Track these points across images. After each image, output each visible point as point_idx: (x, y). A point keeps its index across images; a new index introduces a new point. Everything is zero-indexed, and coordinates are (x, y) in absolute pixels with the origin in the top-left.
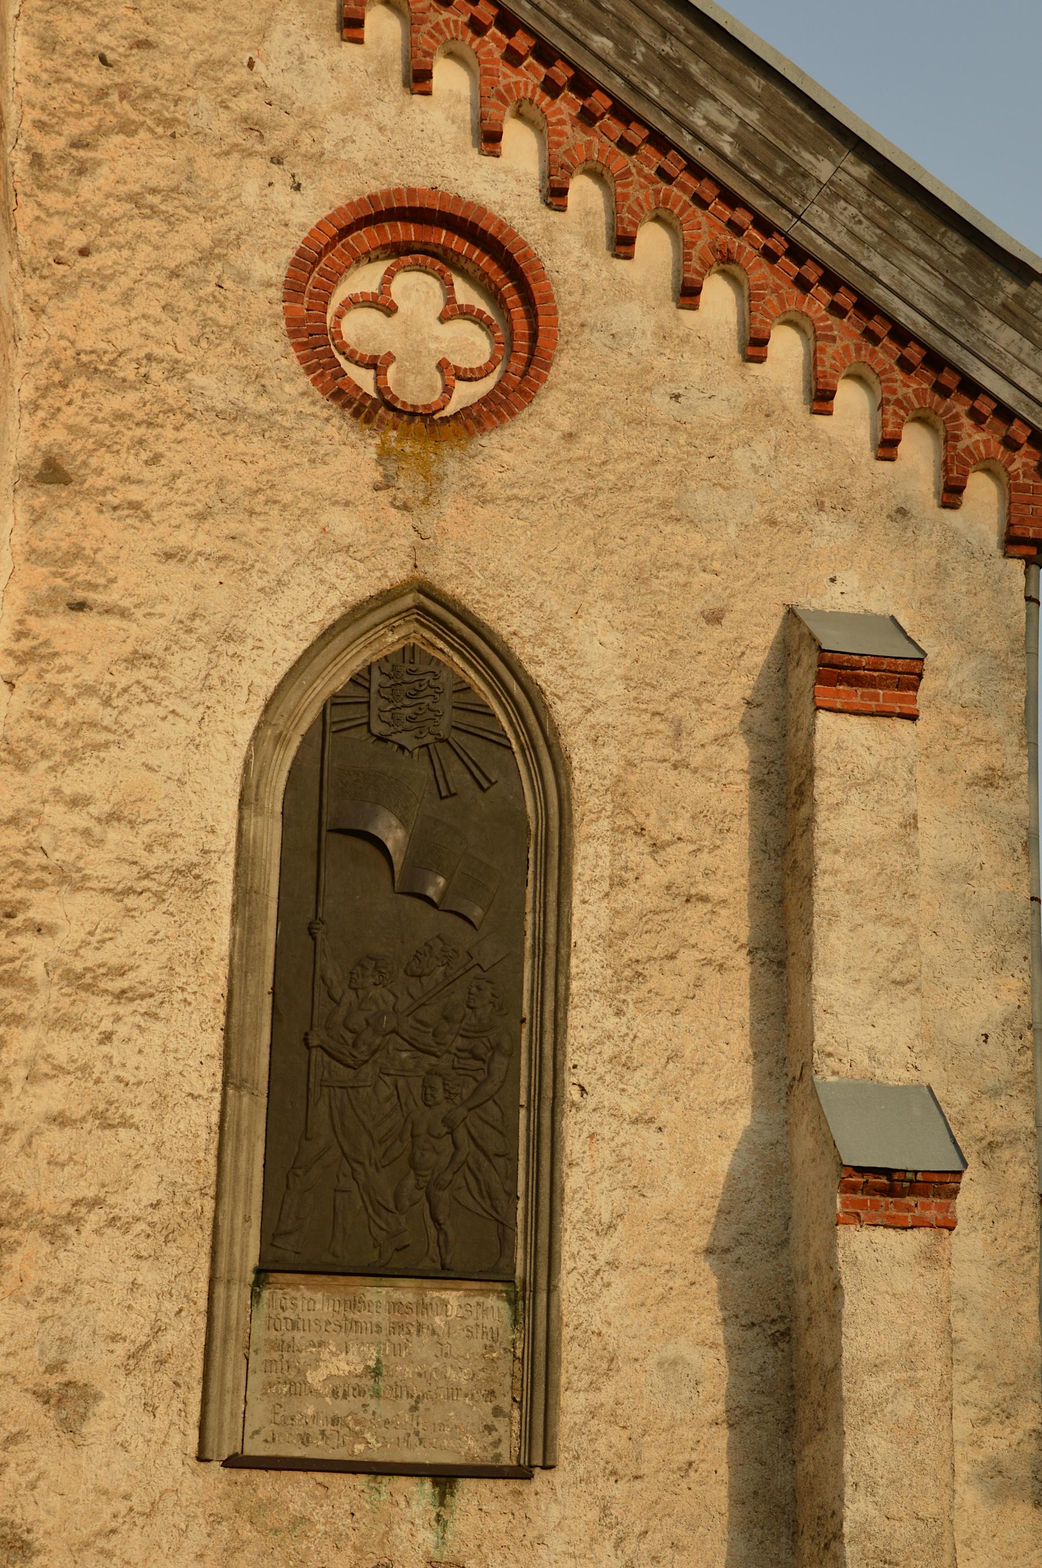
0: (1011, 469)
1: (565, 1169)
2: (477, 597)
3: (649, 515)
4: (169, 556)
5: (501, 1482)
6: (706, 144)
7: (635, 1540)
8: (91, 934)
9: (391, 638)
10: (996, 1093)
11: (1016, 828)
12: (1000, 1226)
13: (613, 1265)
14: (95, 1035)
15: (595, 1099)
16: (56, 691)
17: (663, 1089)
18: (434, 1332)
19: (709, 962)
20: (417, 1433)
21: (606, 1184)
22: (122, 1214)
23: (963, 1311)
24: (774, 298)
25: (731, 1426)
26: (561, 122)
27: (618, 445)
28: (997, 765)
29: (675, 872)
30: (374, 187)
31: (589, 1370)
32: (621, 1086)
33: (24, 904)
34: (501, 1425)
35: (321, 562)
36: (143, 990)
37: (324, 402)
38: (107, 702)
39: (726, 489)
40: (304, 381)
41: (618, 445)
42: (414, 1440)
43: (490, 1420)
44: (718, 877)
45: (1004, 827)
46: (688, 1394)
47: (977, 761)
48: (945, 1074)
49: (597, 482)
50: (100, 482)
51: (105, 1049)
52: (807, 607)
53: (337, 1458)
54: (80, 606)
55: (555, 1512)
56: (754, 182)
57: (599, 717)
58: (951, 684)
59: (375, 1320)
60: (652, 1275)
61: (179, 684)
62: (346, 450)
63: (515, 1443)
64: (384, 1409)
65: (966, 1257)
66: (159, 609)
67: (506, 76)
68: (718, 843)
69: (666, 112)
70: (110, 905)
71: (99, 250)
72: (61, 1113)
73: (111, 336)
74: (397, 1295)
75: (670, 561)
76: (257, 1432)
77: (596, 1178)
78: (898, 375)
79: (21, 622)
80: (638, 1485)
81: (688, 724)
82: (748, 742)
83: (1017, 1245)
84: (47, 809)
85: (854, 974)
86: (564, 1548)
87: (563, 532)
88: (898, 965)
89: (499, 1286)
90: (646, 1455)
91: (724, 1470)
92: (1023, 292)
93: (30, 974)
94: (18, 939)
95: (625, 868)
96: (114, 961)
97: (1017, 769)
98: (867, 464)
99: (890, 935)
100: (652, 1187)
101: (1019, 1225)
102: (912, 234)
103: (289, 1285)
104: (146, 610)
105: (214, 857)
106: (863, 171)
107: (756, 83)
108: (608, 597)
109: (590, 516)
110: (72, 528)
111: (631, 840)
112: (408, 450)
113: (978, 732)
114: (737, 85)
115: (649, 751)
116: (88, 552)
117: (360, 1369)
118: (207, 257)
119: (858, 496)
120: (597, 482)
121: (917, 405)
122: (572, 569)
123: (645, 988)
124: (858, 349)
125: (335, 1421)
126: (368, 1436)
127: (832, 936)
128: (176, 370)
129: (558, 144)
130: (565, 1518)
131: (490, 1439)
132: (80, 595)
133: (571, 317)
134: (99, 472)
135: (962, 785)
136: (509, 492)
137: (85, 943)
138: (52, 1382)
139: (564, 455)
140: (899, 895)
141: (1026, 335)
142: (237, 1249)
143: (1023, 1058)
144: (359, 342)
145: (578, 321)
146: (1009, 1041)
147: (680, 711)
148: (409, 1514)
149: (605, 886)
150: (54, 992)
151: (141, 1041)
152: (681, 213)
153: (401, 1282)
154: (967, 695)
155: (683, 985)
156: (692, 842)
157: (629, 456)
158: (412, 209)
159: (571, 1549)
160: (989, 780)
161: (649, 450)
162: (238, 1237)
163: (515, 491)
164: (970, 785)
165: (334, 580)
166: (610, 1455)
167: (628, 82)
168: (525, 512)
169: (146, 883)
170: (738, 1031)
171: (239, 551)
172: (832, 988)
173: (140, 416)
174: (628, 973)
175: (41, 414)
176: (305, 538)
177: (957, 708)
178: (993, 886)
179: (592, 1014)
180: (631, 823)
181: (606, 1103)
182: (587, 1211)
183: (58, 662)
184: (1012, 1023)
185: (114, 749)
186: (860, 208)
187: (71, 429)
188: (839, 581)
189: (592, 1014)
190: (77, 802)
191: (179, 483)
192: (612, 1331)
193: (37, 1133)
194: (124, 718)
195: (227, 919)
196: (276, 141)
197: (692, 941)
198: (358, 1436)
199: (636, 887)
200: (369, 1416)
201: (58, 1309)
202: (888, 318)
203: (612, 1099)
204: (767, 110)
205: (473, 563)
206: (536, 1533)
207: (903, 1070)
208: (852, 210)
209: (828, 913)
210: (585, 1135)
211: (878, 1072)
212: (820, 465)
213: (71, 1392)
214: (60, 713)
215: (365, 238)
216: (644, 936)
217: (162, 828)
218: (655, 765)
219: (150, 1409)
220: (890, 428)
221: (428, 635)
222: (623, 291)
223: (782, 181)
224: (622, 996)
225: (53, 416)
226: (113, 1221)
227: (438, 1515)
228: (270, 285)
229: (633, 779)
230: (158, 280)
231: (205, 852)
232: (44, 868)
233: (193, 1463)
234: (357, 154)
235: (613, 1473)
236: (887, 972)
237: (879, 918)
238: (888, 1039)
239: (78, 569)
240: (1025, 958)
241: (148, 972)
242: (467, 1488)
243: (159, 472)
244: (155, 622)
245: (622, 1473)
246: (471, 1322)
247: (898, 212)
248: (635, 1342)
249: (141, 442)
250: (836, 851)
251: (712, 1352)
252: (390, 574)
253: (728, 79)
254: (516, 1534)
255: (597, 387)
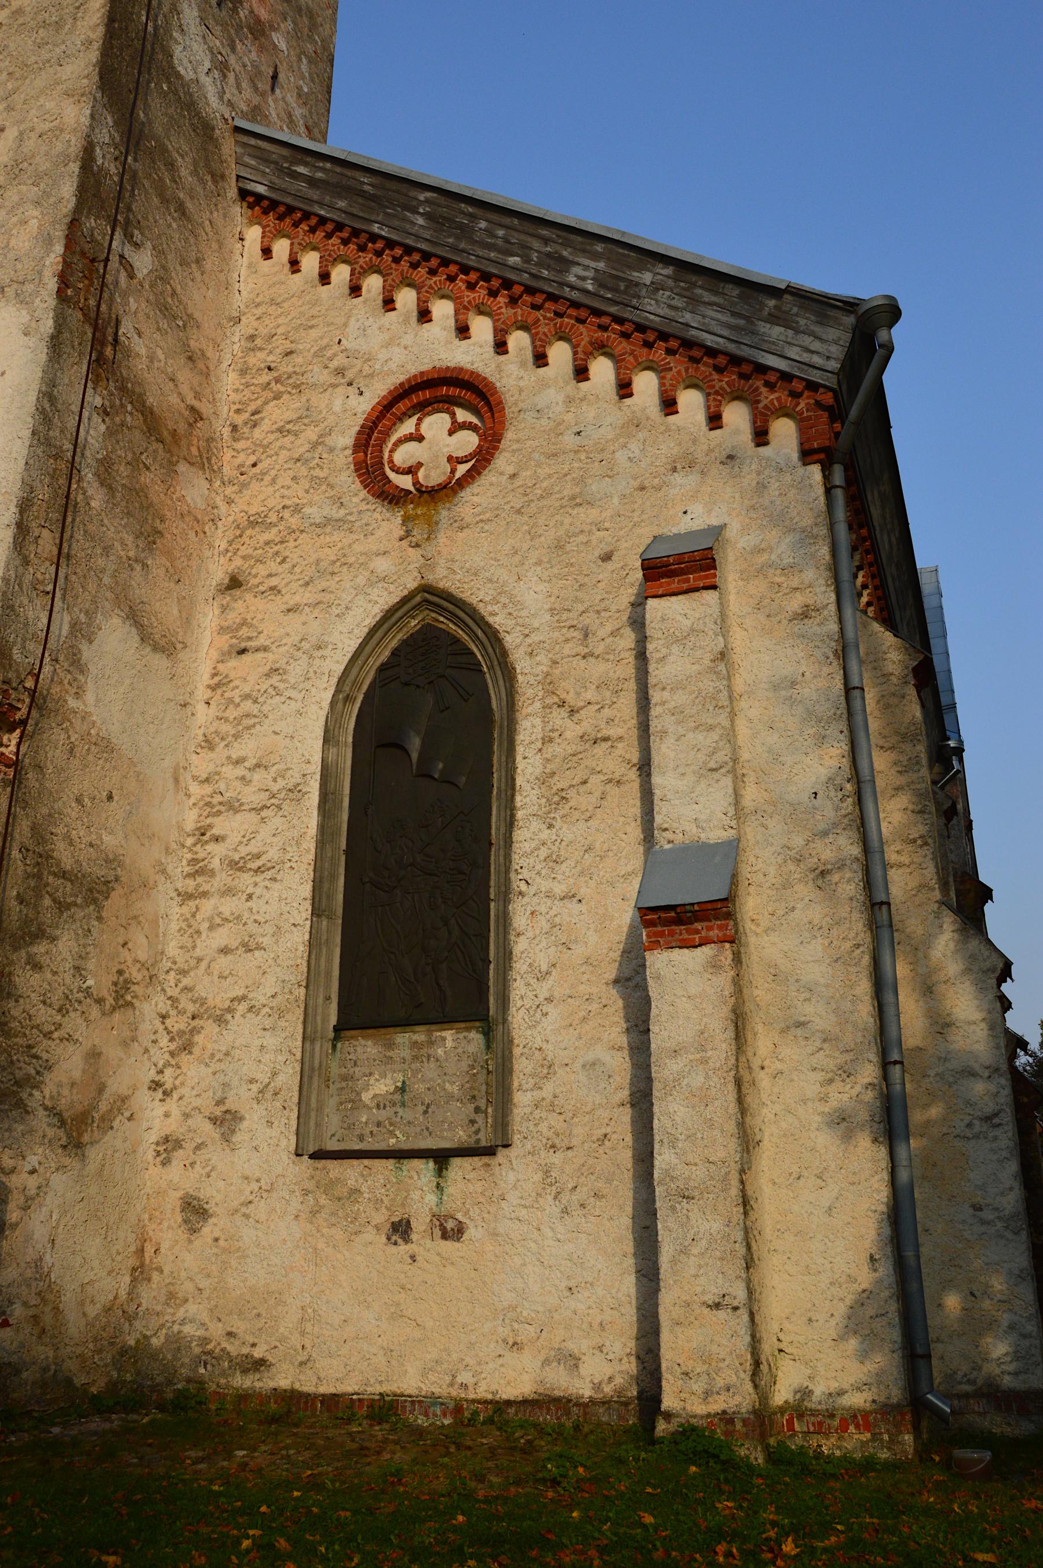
0: (798, 409)
1: (512, 938)
2: (458, 585)
3: (562, 507)
4: (289, 610)
5: (476, 1159)
6: (578, 289)
7: (568, 1193)
8: (244, 837)
9: (413, 623)
10: (825, 834)
11: (828, 641)
12: (834, 932)
13: (549, 1000)
14: (245, 897)
15: (535, 888)
16: (231, 700)
17: (582, 873)
18: (437, 1060)
19: (610, 781)
20: (427, 1129)
21: (544, 944)
22: (257, 1004)
23: (809, 1000)
24: (631, 358)
25: (632, 1105)
26: (501, 308)
27: (542, 472)
28: (811, 602)
29: (586, 726)
30: (402, 378)
31: (533, 1075)
32: (553, 876)
33: (210, 826)
34: (480, 1119)
35: (369, 591)
36: (269, 865)
37: (374, 501)
38: (255, 701)
39: (610, 477)
40: (364, 493)
41: (542, 472)
42: (426, 1133)
43: (473, 1116)
44: (616, 722)
45: (817, 643)
46: (604, 1086)
47: (796, 603)
48: (786, 827)
49: (531, 497)
50: (256, 581)
51: (249, 904)
52: (669, 534)
53: (380, 1148)
54: (243, 651)
55: (512, 1177)
56: (608, 299)
57: (535, 638)
58: (773, 557)
59: (402, 1055)
60: (577, 1004)
61: (293, 681)
62: (385, 523)
63: (489, 1130)
64: (406, 1114)
65: (810, 959)
66: (284, 641)
67: (468, 296)
68: (615, 700)
69: (554, 281)
70: (254, 818)
71: (261, 461)
72: (226, 947)
73: (266, 503)
74: (416, 1037)
75: (577, 531)
76: (333, 1135)
77: (536, 942)
78: (715, 376)
79: (215, 668)
80: (570, 1153)
81: (591, 628)
82: (633, 630)
83: (848, 945)
84: (224, 769)
85: (681, 770)
86: (519, 1201)
87: (510, 532)
88: (714, 757)
89: (477, 1024)
90: (575, 1132)
91: (629, 1139)
92: (779, 303)
93: (212, 866)
94: (207, 847)
95: (552, 731)
96: (255, 851)
97: (826, 602)
98: (704, 435)
99: (705, 738)
100: (576, 942)
101: (850, 929)
102: (705, 294)
103: (352, 1038)
104: (277, 644)
105: (309, 777)
106: (669, 271)
107: (599, 248)
108: (539, 563)
109: (526, 518)
110: (242, 610)
111: (556, 712)
112: (419, 512)
113: (795, 583)
114: (589, 252)
115: (567, 651)
116: (249, 620)
117: (392, 1089)
118: (315, 445)
119: (699, 456)
120: (531, 497)
121: (729, 390)
122: (516, 553)
123: (567, 807)
124: (687, 370)
125: (379, 1124)
126: (397, 1133)
127: (663, 746)
128: (297, 509)
129: (499, 320)
130: (518, 1181)
131: (473, 1129)
132: (243, 645)
133: (513, 409)
134: (255, 576)
135: (785, 622)
136: (477, 519)
137: (241, 843)
138: (218, 1111)
139: (510, 487)
140: (711, 708)
141: (787, 327)
142: (319, 1018)
143: (844, 805)
144: (404, 462)
145: (517, 409)
146: (832, 794)
147: (587, 621)
148: (419, 1183)
149: (539, 745)
150: (224, 874)
151: (268, 896)
152: (570, 331)
153: (417, 1028)
154: (785, 562)
155: (594, 800)
156: (597, 703)
157: (550, 476)
158: (423, 382)
159: (523, 1202)
160: (805, 614)
161: (563, 469)
162: (320, 1010)
163: (481, 517)
164: (790, 621)
165: (376, 598)
166: (550, 1134)
167: (530, 274)
168: (486, 527)
169: (273, 801)
170: (633, 824)
171: (327, 597)
172: (666, 782)
173: (278, 539)
174: (556, 799)
175: (229, 554)
176: (361, 580)
177: (779, 571)
178: (812, 686)
179: (532, 831)
180: (556, 699)
181: (543, 889)
182: (530, 965)
183: (231, 685)
184: (834, 780)
185: (258, 726)
186: (672, 291)
187: (243, 557)
188: (689, 512)
189: (532, 831)
190: (239, 762)
191: (296, 569)
192: (550, 1047)
193: (214, 960)
194: (264, 707)
195: (315, 813)
196: (350, 375)
197: (598, 769)
198: (392, 1134)
199: (560, 741)
200: (398, 1119)
201: (223, 1066)
202: (702, 346)
203: (545, 885)
204: (608, 259)
205: (456, 567)
206: (500, 1192)
207: (722, 830)
208: (668, 293)
209: (660, 731)
210: (528, 912)
211: (703, 836)
212: (672, 445)
213: (228, 1116)
214: (232, 713)
215: (401, 406)
216: (567, 772)
217: (282, 766)
218: (570, 659)
219: (270, 1123)
220: (712, 409)
221: (434, 615)
222: (544, 384)
223: (625, 292)
224: (552, 815)
225: (235, 553)
226: (251, 1009)
227: (438, 1184)
228: (346, 449)
229: (557, 671)
230: (290, 466)
231: (304, 775)
232: (221, 803)
233: (293, 1157)
234: (393, 365)
235: (553, 1146)
236: (705, 763)
237: (697, 728)
238: (708, 811)
239: (244, 632)
240: (842, 732)
241: (273, 854)
242: (457, 1164)
243: (286, 566)
244: (283, 649)
245: (559, 1146)
246: (460, 1050)
247: (694, 285)
248: (566, 1052)
249: (277, 553)
250: (664, 689)
251: (619, 1053)
252: (408, 586)
253: (584, 251)
254: (486, 1193)
255: (529, 443)
